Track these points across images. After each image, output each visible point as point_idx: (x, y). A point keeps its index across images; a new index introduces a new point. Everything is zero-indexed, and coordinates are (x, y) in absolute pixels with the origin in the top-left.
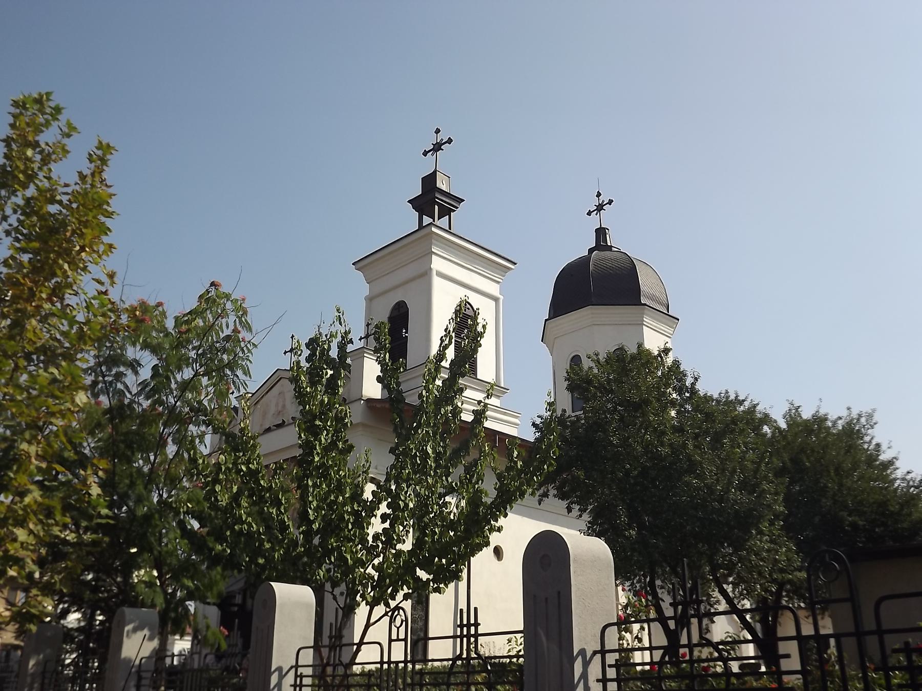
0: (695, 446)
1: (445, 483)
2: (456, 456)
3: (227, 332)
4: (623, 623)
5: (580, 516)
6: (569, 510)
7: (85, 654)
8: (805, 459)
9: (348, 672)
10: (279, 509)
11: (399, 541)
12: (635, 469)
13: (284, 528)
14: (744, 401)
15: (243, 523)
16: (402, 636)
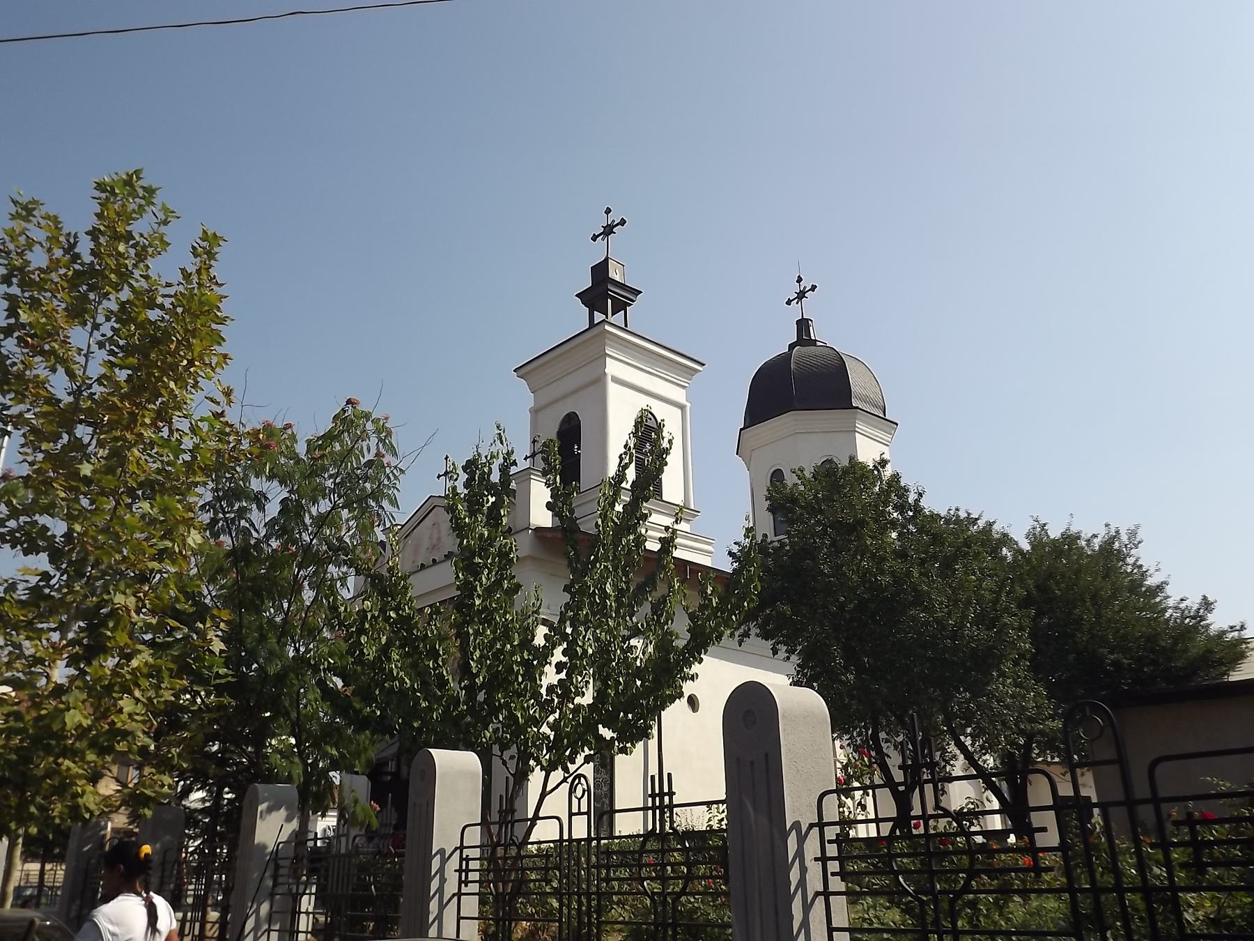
0: (921, 574)
1: (630, 624)
2: (641, 591)
3: (369, 457)
4: (843, 789)
5: (788, 658)
6: (775, 652)
7: (211, 838)
8: (1054, 587)
9: (522, 853)
10: (436, 661)
11: (577, 694)
12: (851, 602)
13: (443, 683)
15: (395, 679)
16: (584, 809)
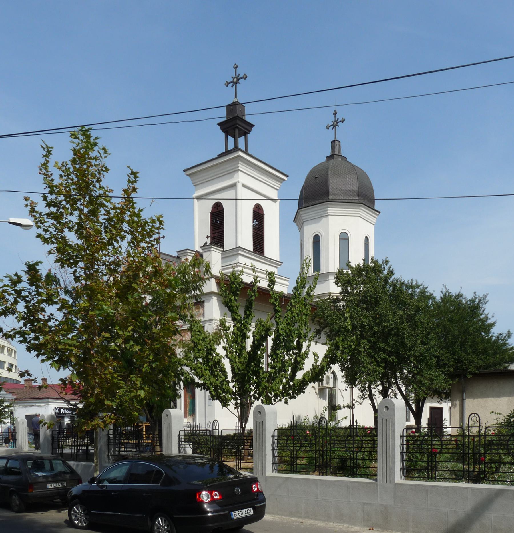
14: (420, 286)
